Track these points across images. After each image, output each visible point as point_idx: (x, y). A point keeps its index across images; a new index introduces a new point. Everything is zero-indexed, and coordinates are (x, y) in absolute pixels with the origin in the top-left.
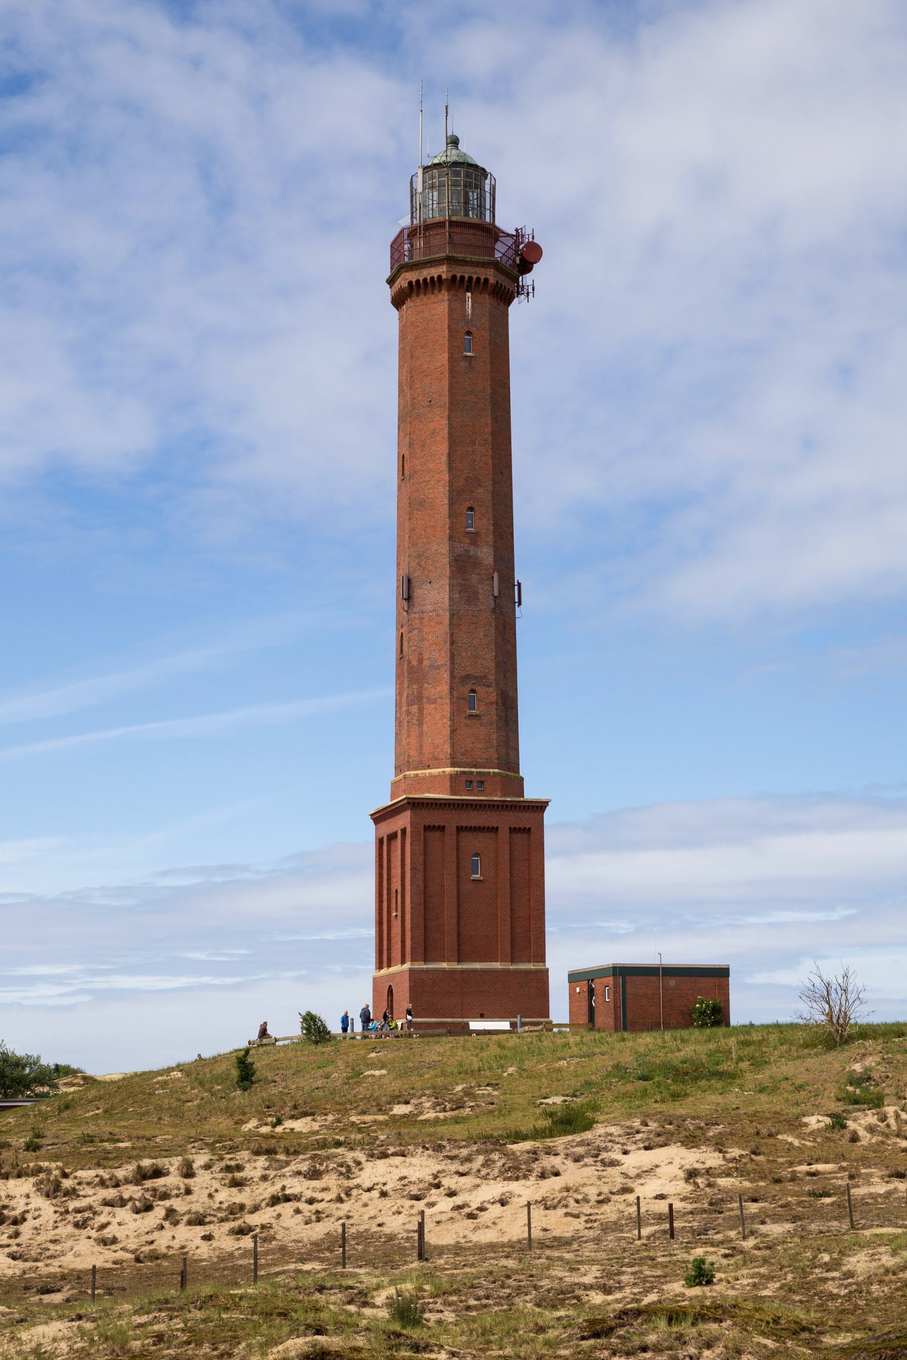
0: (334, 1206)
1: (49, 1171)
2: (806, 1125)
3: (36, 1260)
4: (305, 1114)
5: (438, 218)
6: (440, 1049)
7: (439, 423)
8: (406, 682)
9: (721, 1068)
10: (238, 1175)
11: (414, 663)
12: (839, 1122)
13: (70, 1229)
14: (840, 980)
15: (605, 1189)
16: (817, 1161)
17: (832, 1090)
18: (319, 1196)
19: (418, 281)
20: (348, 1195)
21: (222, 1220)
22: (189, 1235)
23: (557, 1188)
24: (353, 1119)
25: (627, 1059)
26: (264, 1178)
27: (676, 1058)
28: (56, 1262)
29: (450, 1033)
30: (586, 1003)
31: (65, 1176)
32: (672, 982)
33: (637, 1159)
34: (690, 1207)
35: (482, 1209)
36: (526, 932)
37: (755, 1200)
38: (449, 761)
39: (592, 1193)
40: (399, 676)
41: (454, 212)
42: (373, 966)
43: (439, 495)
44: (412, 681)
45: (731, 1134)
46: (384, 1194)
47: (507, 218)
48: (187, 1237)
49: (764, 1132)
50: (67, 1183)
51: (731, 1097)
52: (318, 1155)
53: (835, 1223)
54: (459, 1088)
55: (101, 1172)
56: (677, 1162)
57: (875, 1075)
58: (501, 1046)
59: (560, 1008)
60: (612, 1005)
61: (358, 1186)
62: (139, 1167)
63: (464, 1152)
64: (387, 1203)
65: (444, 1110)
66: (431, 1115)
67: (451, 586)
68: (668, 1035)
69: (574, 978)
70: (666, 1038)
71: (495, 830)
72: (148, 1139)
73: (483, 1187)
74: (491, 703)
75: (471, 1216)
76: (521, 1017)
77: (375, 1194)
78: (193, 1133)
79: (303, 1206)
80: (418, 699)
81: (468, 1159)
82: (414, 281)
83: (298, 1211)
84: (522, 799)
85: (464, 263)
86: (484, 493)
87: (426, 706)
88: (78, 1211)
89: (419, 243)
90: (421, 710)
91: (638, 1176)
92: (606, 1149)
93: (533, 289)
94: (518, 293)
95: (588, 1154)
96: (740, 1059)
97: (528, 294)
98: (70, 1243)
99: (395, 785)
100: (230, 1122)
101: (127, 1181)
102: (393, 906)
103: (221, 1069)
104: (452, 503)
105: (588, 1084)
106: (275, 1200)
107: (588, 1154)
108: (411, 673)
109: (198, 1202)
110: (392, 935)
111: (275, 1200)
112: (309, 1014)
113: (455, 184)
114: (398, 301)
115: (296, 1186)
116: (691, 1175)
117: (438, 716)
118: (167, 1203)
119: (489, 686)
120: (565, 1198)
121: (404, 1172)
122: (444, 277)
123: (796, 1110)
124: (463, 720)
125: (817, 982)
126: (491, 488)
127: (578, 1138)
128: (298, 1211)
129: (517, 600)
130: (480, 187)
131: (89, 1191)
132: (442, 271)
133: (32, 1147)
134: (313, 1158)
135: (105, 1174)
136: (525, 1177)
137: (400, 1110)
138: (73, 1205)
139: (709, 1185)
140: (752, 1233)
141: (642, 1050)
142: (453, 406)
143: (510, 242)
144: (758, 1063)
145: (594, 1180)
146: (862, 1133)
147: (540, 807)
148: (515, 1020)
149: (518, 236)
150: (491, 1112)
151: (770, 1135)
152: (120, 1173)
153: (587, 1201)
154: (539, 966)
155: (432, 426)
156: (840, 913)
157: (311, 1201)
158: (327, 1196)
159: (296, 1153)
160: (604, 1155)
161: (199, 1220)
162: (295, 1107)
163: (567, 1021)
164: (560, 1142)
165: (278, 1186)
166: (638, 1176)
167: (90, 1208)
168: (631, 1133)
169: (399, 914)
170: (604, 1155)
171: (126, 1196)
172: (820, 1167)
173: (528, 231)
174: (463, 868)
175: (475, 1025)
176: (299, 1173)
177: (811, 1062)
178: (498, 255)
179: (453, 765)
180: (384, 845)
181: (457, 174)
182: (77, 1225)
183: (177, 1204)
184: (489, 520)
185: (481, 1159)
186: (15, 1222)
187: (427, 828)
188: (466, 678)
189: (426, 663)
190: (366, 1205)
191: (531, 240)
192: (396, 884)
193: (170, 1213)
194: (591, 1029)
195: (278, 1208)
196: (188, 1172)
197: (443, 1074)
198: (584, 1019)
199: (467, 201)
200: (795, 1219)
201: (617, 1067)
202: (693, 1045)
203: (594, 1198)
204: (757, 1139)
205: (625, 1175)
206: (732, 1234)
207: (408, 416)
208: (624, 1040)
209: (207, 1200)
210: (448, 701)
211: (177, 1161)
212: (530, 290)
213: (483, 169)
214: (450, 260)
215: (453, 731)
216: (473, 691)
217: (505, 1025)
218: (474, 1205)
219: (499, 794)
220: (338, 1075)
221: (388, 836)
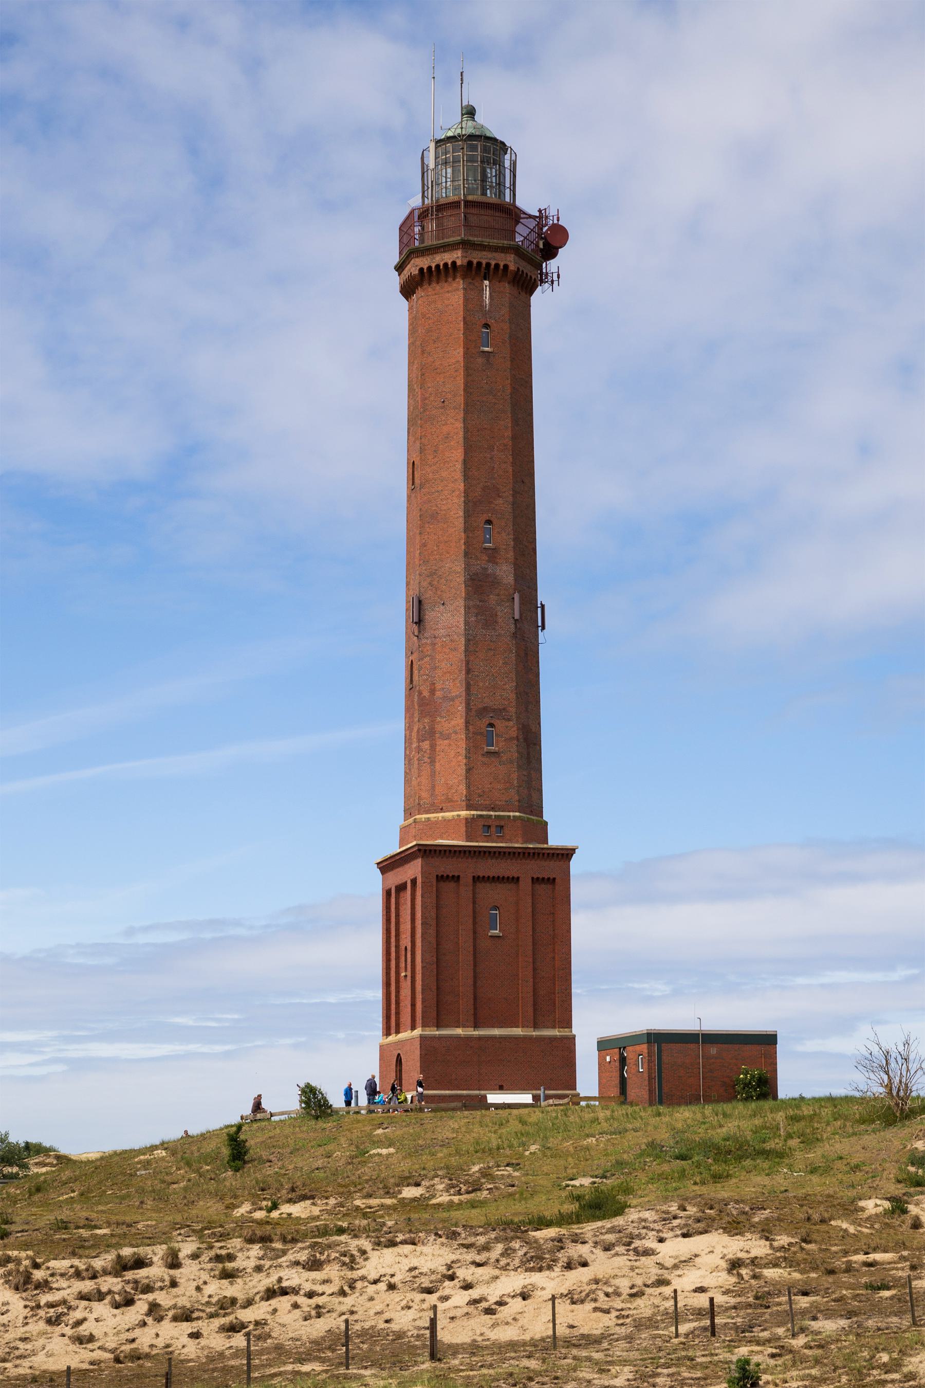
0: (336, 1300)
1: (18, 1261)
2: (863, 1209)
4: (304, 1198)
5: (452, 198)
6: (454, 1126)
7: (454, 425)
8: (416, 715)
9: (768, 1146)
10: (230, 1265)
11: (426, 694)
12: (899, 1206)
13: (42, 1325)
15: (639, 1281)
16: (875, 1250)
17: (892, 1171)
18: (319, 1288)
19: (430, 268)
20: (352, 1287)
21: (211, 1316)
23: (585, 1279)
24: (358, 1203)
25: (663, 1136)
26: (259, 1269)
28: (26, 1363)
29: (466, 1107)
30: (617, 1074)
31: (36, 1266)
32: (713, 1050)
33: (675, 1248)
34: (733, 1301)
35: (501, 1303)
36: (551, 995)
37: (805, 1294)
38: (464, 803)
39: (624, 1285)
40: (408, 709)
41: (470, 191)
42: (379, 1032)
43: (453, 505)
44: (422, 714)
45: (779, 1220)
46: (392, 1287)
47: (529, 197)
48: (172, 1334)
49: (816, 1217)
50: (38, 1275)
51: (779, 1179)
53: (895, 1319)
54: (476, 1168)
55: (76, 1262)
56: (719, 1251)
58: (523, 1122)
59: (588, 1079)
60: (646, 1075)
61: (363, 1278)
62: (119, 1256)
63: (481, 1240)
64: (395, 1296)
65: (459, 1193)
66: (444, 1198)
67: (467, 608)
68: (708, 1109)
69: (603, 1045)
71: (516, 880)
72: (129, 1226)
73: (503, 1278)
74: (511, 739)
75: (489, 1311)
76: (545, 1089)
77: (382, 1286)
78: (178, 1218)
79: (301, 1300)
80: (430, 734)
81: (486, 1248)
82: (425, 268)
83: (296, 1306)
84: (545, 846)
85: (481, 249)
86: (503, 504)
87: (439, 742)
88: (51, 1305)
89: (431, 225)
90: (433, 747)
91: (676, 1267)
92: (640, 1237)
93: (558, 277)
94: (542, 281)
95: (619, 1242)
96: (789, 1136)
97: (552, 282)
98: (42, 1341)
99: (404, 830)
100: (220, 1206)
101: (105, 1272)
102: (402, 965)
103: (209, 1147)
104: (467, 515)
105: (620, 1164)
106: (270, 1294)
107: (619, 1242)
108: (422, 705)
109: (185, 1296)
110: (401, 998)
111: (270, 1294)
112: (308, 1086)
113: (471, 159)
114: (407, 290)
115: (294, 1277)
116: (735, 1265)
117: (452, 754)
118: (150, 1297)
119: (509, 720)
120: (594, 1291)
121: (414, 1262)
122: (459, 263)
123: (851, 1193)
124: (480, 758)
125: (875, 1050)
126: (511, 499)
127: (608, 1224)
128: (296, 1306)
129: (540, 624)
130: (499, 163)
131: (63, 1283)
132: (456, 256)
135: (80, 1264)
136: (550, 1268)
137: (409, 1192)
138: (44, 1299)
139: (755, 1277)
140: (803, 1330)
142: (469, 407)
143: (532, 224)
144: (809, 1141)
145: (625, 1271)
147: (566, 854)
148: (538, 1092)
149: (541, 217)
150: (511, 1195)
151: (823, 1221)
152: (98, 1264)
153: (617, 1294)
155: (445, 429)
156: (901, 973)
157: (310, 1295)
159: (294, 1241)
160: (637, 1243)
161: (185, 1316)
162: (293, 1190)
163: (595, 1093)
164: (588, 1229)
165: (274, 1278)
166: (676, 1267)
167: (64, 1302)
169: (409, 974)
170: (637, 1243)
171: (104, 1289)
173: (552, 212)
174: (480, 922)
176: (297, 1263)
177: (869, 1140)
178: (519, 239)
179: (469, 807)
181: (473, 148)
182: (49, 1321)
184: (508, 534)
185: (499, 1248)
187: (440, 878)
188: (483, 711)
190: (371, 1299)
191: (555, 222)
192: (406, 941)
193: (153, 1308)
194: (623, 1103)
195: (274, 1302)
196: (174, 1263)
197: (458, 1152)
198: (615, 1092)
199: (484, 178)
200: (850, 1314)
201: (652, 1145)
202: (737, 1120)
203: (626, 1291)
205: (661, 1265)
206: (780, 1331)
207: (420, 418)
209: (194, 1293)
210: (463, 736)
212: (555, 278)
213: (503, 143)
214: (465, 245)
215: (469, 770)
217: (527, 1098)
218: (493, 1299)
219: (520, 840)
220: (341, 1154)
221: (396, 887)
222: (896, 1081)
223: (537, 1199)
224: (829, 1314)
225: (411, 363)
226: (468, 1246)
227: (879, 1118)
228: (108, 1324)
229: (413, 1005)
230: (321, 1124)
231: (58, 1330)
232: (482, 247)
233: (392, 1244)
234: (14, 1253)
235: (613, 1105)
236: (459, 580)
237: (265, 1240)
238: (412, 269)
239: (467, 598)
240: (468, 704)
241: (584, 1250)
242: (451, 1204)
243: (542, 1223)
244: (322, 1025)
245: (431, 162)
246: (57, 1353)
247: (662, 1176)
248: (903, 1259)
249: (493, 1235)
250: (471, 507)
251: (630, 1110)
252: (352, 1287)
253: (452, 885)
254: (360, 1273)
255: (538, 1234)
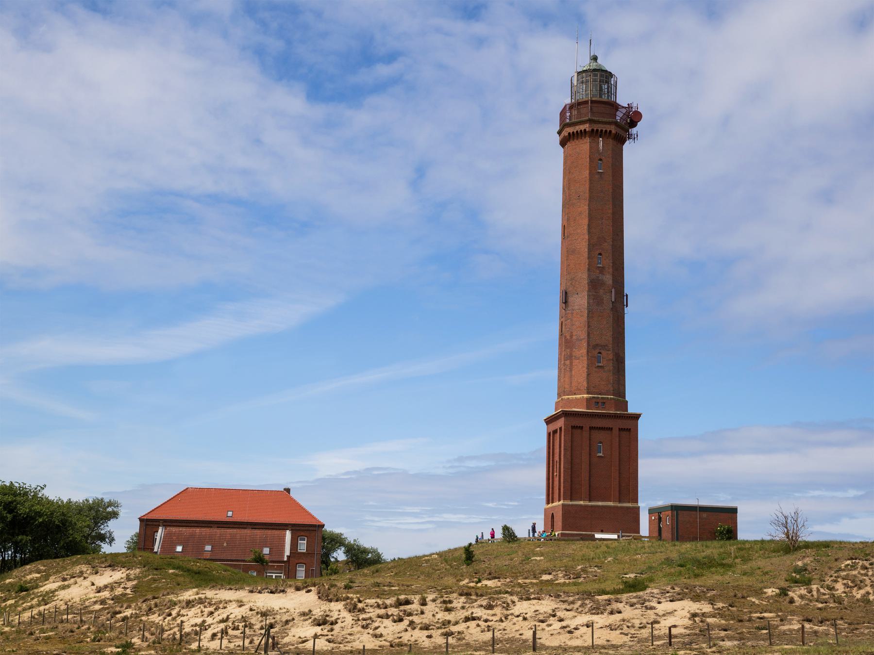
0: (497, 623)
1: (352, 599)
2: (765, 593)
3: (340, 643)
4: (495, 578)
5: (585, 99)
6: (576, 548)
7: (584, 208)
9: (724, 562)
10: (449, 605)
11: (568, 337)
12: (784, 592)
13: (359, 628)
14: (793, 515)
15: (644, 621)
16: (765, 612)
17: (784, 575)
18: (490, 618)
20: (506, 618)
21: (438, 628)
22: (420, 635)
23: (618, 619)
24: (520, 581)
25: (674, 555)
26: (463, 608)
27: (700, 556)
28: (350, 645)
29: (582, 539)
30: (657, 525)
31: (360, 601)
32: (705, 515)
33: (666, 606)
34: (688, 632)
35: (576, 629)
36: (628, 487)
37: (725, 630)
39: (637, 623)
40: (560, 345)
41: (594, 96)
42: (545, 501)
43: (583, 246)
44: (567, 347)
45: (720, 595)
46: (525, 619)
47: (622, 99)
48: (419, 635)
49: (740, 595)
50: (360, 605)
51: (727, 577)
52: (492, 599)
53: (762, 642)
54: (579, 567)
55: (378, 601)
56: (687, 609)
57: (809, 568)
58: (608, 547)
59: (644, 529)
61: (512, 614)
62: (398, 599)
63: (571, 599)
64: (526, 623)
65: (570, 578)
66: (562, 581)
67: (589, 296)
68: (699, 544)
69: (651, 511)
70: (698, 545)
71: (611, 429)
72: (408, 586)
73: (579, 617)
75: (570, 632)
77: (521, 618)
78: (433, 584)
79: (481, 623)
80: (570, 357)
81: (573, 603)
83: (478, 625)
85: (600, 123)
86: (607, 246)
88: (364, 619)
89: (575, 112)
90: (571, 363)
91: (664, 615)
92: (649, 601)
94: (629, 138)
95: (638, 603)
96: (736, 557)
98: (358, 636)
99: (557, 404)
100: (454, 580)
101: (391, 606)
103: (457, 554)
104: (590, 251)
105: (650, 568)
106: (467, 619)
107: (638, 603)
108: (566, 342)
109: (427, 618)
111: (467, 619)
112: (505, 526)
113: (595, 81)
114: (563, 143)
115: (478, 612)
116: (694, 615)
118: (411, 618)
120: (621, 625)
121: (537, 608)
123: (760, 585)
125: (780, 515)
127: (634, 594)
128: (478, 625)
130: (608, 82)
131: (371, 610)
132: (586, 127)
133: (347, 587)
134: (489, 599)
135: (380, 602)
136: (602, 613)
137: (545, 577)
138: (362, 616)
139: (702, 621)
140: (715, 645)
141: (683, 551)
142: (591, 199)
144: (745, 560)
145: (639, 616)
146: (796, 598)
147: (637, 417)
149: (630, 107)
150: (594, 580)
151: (743, 597)
152: (388, 602)
153: (633, 627)
154: (634, 505)
156: (852, 493)
157: (486, 621)
158: (495, 619)
159: (482, 595)
160: (647, 604)
161: (426, 628)
162: (490, 574)
163: (647, 535)
164: (624, 597)
165: (469, 612)
166: (664, 615)
167: (370, 618)
168: (664, 593)
170: (647, 604)
171: (390, 613)
172: (766, 615)
173: (635, 105)
174: (594, 449)
175: (597, 536)
176: (482, 606)
177: (775, 560)
178: (618, 118)
180: (551, 436)
181: (596, 75)
182: (363, 627)
183: (416, 619)
185: (580, 602)
186: (332, 624)
187: (573, 427)
188: (596, 346)
189: (574, 337)
190: (514, 624)
192: (557, 458)
193: (412, 623)
194: (660, 539)
195: (468, 623)
196: (424, 603)
197: (573, 560)
198: (656, 534)
199: (601, 89)
200: (740, 639)
201: (667, 559)
202: (713, 549)
203: (637, 625)
204: (734, 599)
205: (657, 614)
206: (704, 645)
207: (568, 204)
208: (675, 545)
209: (431, 617)
211: (418, 597)
214: (590, 121)
215: (588, 375)
216: (600, 353)
217: (615, 536)
218: (572, 627)
220: (517, 559)
222: (791, 532)
223: (607, 583)
224: (730, 638)
225: (564, 178)
226: (564, 602)
227: (782, 550)
228: (390, 629)
229: (560, 489)
230: (511, 545)
231: (367, 631)
232: (599, 122)
233: (529, 599)
234: (351, 595)
235: (654, 540)
236: (585, 282)
237: (468, 594)
238: (565, 133)
239: (589, 291)
240: (588, 343)
241: (620, 606)
242: (564, 584)
243: (604, 592)
244: (520, 499)
245: (575, 83)
246: (366, 641)
247: (670, 574)
248: (778, 616)
249: (577, 597)
250: (591, 247)
251: (661, 543)
252: (506, 618)
253: (579, 431)
254: (511, 612)
255: (599, 597)
